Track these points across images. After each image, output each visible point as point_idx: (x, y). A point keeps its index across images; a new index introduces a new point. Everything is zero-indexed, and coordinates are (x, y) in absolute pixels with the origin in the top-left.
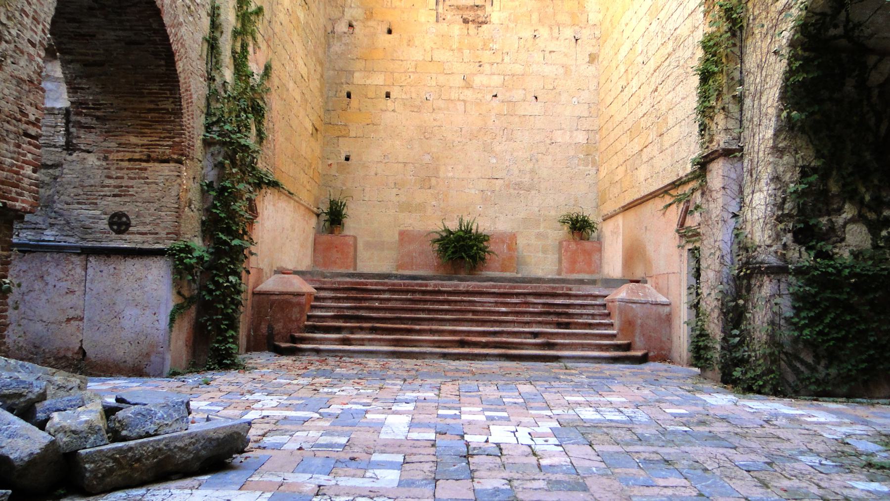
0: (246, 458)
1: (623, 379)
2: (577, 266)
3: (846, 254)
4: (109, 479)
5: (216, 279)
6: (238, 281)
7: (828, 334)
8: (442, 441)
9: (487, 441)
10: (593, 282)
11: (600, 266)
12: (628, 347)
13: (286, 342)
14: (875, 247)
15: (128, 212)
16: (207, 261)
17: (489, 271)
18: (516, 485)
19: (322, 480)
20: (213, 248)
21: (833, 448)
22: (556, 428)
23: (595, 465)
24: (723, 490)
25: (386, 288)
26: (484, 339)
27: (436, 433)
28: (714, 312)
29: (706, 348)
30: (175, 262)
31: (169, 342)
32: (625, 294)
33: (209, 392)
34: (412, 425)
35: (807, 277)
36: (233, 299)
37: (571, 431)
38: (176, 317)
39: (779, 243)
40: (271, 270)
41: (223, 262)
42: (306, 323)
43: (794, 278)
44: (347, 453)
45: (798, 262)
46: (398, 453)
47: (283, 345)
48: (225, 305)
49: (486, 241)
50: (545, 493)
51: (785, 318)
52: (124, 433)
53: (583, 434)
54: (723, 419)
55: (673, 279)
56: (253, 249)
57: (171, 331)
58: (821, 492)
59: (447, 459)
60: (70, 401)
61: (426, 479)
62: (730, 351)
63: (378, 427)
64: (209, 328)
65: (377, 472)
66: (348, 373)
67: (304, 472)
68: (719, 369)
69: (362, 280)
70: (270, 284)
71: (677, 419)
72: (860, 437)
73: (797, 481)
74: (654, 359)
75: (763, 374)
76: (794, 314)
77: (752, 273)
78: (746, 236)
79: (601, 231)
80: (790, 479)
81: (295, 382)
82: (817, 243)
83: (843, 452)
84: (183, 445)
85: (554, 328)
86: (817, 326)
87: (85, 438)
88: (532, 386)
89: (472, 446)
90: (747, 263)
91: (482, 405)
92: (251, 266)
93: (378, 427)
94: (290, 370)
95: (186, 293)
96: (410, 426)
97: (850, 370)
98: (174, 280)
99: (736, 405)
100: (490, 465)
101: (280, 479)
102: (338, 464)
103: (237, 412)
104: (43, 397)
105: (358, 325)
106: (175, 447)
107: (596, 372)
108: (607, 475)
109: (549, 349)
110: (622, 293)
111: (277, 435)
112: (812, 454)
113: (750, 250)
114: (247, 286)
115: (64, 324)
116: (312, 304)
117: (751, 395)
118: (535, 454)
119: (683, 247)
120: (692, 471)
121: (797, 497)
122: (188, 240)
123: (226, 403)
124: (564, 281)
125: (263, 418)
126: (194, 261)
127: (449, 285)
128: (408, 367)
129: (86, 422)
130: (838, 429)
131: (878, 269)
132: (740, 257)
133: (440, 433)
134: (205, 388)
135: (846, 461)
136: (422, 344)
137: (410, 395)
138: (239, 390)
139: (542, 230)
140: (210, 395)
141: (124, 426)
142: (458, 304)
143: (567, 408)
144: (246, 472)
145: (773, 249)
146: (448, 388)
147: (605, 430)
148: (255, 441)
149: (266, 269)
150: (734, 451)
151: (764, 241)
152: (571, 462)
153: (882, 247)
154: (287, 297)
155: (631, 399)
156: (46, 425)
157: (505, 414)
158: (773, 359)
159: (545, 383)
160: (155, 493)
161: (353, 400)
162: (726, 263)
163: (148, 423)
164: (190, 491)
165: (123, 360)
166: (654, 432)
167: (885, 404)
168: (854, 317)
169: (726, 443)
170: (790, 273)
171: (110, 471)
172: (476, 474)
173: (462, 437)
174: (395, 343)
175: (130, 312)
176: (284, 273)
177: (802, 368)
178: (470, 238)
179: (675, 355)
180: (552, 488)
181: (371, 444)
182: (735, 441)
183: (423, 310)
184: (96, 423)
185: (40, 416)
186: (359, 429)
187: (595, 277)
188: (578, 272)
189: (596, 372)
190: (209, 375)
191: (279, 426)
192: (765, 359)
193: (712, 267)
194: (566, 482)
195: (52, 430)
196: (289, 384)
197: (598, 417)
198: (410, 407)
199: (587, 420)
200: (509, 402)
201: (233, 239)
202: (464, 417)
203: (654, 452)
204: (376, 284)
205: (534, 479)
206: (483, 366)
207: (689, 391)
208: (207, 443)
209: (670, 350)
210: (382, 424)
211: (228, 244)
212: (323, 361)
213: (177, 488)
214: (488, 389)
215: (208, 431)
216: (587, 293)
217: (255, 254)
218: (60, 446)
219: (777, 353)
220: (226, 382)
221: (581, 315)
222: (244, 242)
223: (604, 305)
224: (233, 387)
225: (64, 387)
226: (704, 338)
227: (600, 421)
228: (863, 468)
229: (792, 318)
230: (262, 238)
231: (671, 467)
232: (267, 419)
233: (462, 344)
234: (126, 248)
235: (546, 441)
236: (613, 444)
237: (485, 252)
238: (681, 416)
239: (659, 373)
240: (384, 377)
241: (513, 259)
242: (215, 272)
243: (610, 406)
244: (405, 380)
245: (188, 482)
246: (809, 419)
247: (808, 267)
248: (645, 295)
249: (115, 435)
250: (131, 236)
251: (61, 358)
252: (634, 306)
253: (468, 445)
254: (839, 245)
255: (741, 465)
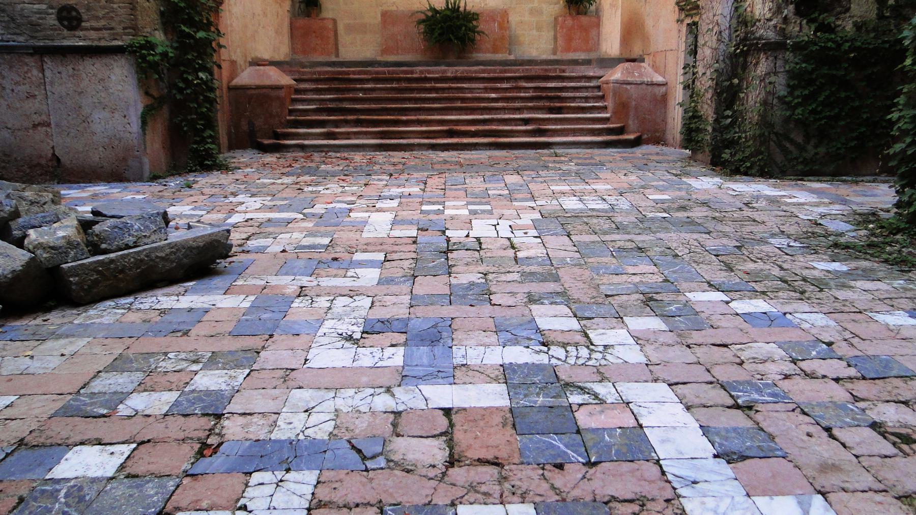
0: (230, 263)
1: (612, 165)
2: (574, 44)
3: (849, 27)
4: (95, 290)
5: (185, 76)
6: (209, 77)
7: (820, 112)
8: (423, 238)
9: (467, 236)
10: (588, 62)
11: (598, 44)
12: (621, 131)
13: (269, 138)
14: (881, 17)
15: (76, 5)
16: (172, 57)
17: (479, 53)
18: (491, 278)
19: (305, 282)
20: (177, 42)
21: (805, 230)
22: (538, 220)
23: (571, 255)
24: (689, 275)
25: (370, 77)
26: (473, 128)
27: (418, 230)
28: (708, 92)
29: (698, 130)
30: (137, 60)
31: (145, 145)
32: (619, 75)
33: (191, 196)
34: (395, 223)
35: (805, 52)
36: (206, 97)
37: (552, 222)
38: (148, 120)
39: (779, 16)
40: (245, 61)
41: (189, 57)
42: (288, 118)
43: (791, 54)
44: (329, 253)
45: (797, 36)
46: (379, 251)
47: (266, 142)
48: (198, 104)
49: (476, 20)
50: (518, 285)
51: (779, 98)
52: (104, 246)
53: (562, 224)
54: (704, 204)
55: (671, 57)
56: (222, 41)
57: (145, 134)
58: (782, 273)
59: (427, 255)
60: (44, 217)
61: (405, 276)
62: (721, 133)
63: (360, 226)
64: (185, 129)
65: (358, 271)
66: (333, 169)
67: (287, 274)
68: (710, 151)
69: (344, 69)
70: (246, 77)
71: (659, 205)
72: (833, 217)
73: (762, 263)
74: (648, 142)
75: (752, 155)
76: (788, 93)
77: (749, 50)
78: (746, 10)
79: (600, 4)
80: (755, 262)
81: (279, 181)
82: (819, 15)
83: (813, 233)
84: (164, 255)
85: (546, 114)
86: (810, 105)
87: (65, 253)
88: (519, 177)
89: (453, 241)
90: (745, 39)
91: (466, 199)
92: (223, 58)
93: (360, 226)
94: (274, 169)
95: (155, 93)
96: (393, 224)
97: (839, 149)
98: (139, 80)
99: (720, 188)
100: (468, 260)
101: (263, 283)
102: (321, 265)
103: (221, 216)
104: (16, 214)
105: (342, 118)
106: (157, 257)
107: (586, 159)
108: (580, 265)
109: (540, 136)
110: (617, 74)
111: (261, 238)
112: (782, 237)
113: (749, 25)
114: (222, 82)
115: (31, 131)
116: (293, 97)
117: (738, 177)
118: (513, 247)
119: (682, 21)
120: (662, 258)
121: (757, 279)
122: (148, 35)
123: (209, 206)
124: (556, 62)
125: (246, 221)
126: (157, 58)
127: (436, 71)
128: (395, 160)
129: (64, 237)
130: (815, 209)
131: (880, 41)
132: (739, 32)
133: (422, 230)
134: (188, 192)
135: (814, 242)
136: (409, 135)
137: (395, 191)
138: (222, 192)
139: (536, 5)
140: (193, 199)
141: (103, 240)
142: (446, 91)
143: (550, 198)
144: (231, 277)
145: (772, 23)
146: (434, 181)
147: (585, 220)
148: (239, 246)
149: (240, 61)
150: (708, 236)
151: (764, 15)
152: (547, 254)
153: (887, 17)
154: (264, 90)
155: (616, 185)
156: (23, 242)
157: (488, 207)
158: (762, 139)
159: (533, 173)
160: (142, 301)
161: (337, 199)
162: (723, 40)
163: (126, 235)
164: (176, 298)
165: (100, 165)
166: (633, 219)
167: (869, 182)
168: (848, 94)
169: (701, 229)
170: (788, 49)
171: (96, 283)
172: (454, 269)
173: (444, 232)
174: (378, 136)
175: (99, 116)
176: (259, 65)
177: (791, 148)
178: (458, 18)
179: (669, 137)
180: (525, 280)
181: (354, 243)
182: (711, 225)
183: (410, 100)
184: (73, 238)
185: (17, 233)
186: (343, 228)
187: (593, 56)
188: (575, 51)
189: (586, 159)
190: (191, 178)
191: (262, 228)
192: (755, 140)
193: (709, 44)
194: (539, 273)
195: (31, 247)
196: (274, 183)
197: (581, 206)
198: (394, 203)
199: (569, 209)
200: (494, 195)
201: (198, 31)
202: (447, 212)
203: (629, 240)
204: (359, 73)
205: (509, 272)
206: (472, 157)
207: (676, 175)
208: (188, 252)
209: (664, 132)
210: (365, 222)
211: (193, 37)
212: (308, 157)
213: (164, 295)
214: (474, 181)
215: (187, 241)
216: (581, 74)
217: (224, 47)
218: (41, 261)
219: (766, 134)
220: (208, 185)
221: (574, 99)
222: (210, 34)
223: (599, 88)
224: (217, 190)
225: (38, 203)
226: (697, 120)
227: (581, 211)
228: (829, 248)
229: (786, 97)
230: (231, 25)
231: (643, 254)
232: (250, 221)
233: (451, 134)
234: (81, 46)
235: (526, 233)
236: (591, 234)
237: (474, 32)
238: (663, 202)
239: (650, 157)
240: (370, 172)
241: (507, 40)
242: (182, 68)
243: (595, 194)
244: (391, 175)
245: (175, 289)
246: (789, 200)
247: (807, 42)
248: (641, 75)
249: (96, 250)
250: (84, 32)
251: (35, 166)
252: (628, 87)
253: (448, 240)
254: (843, 16)
255: (711, 250)
